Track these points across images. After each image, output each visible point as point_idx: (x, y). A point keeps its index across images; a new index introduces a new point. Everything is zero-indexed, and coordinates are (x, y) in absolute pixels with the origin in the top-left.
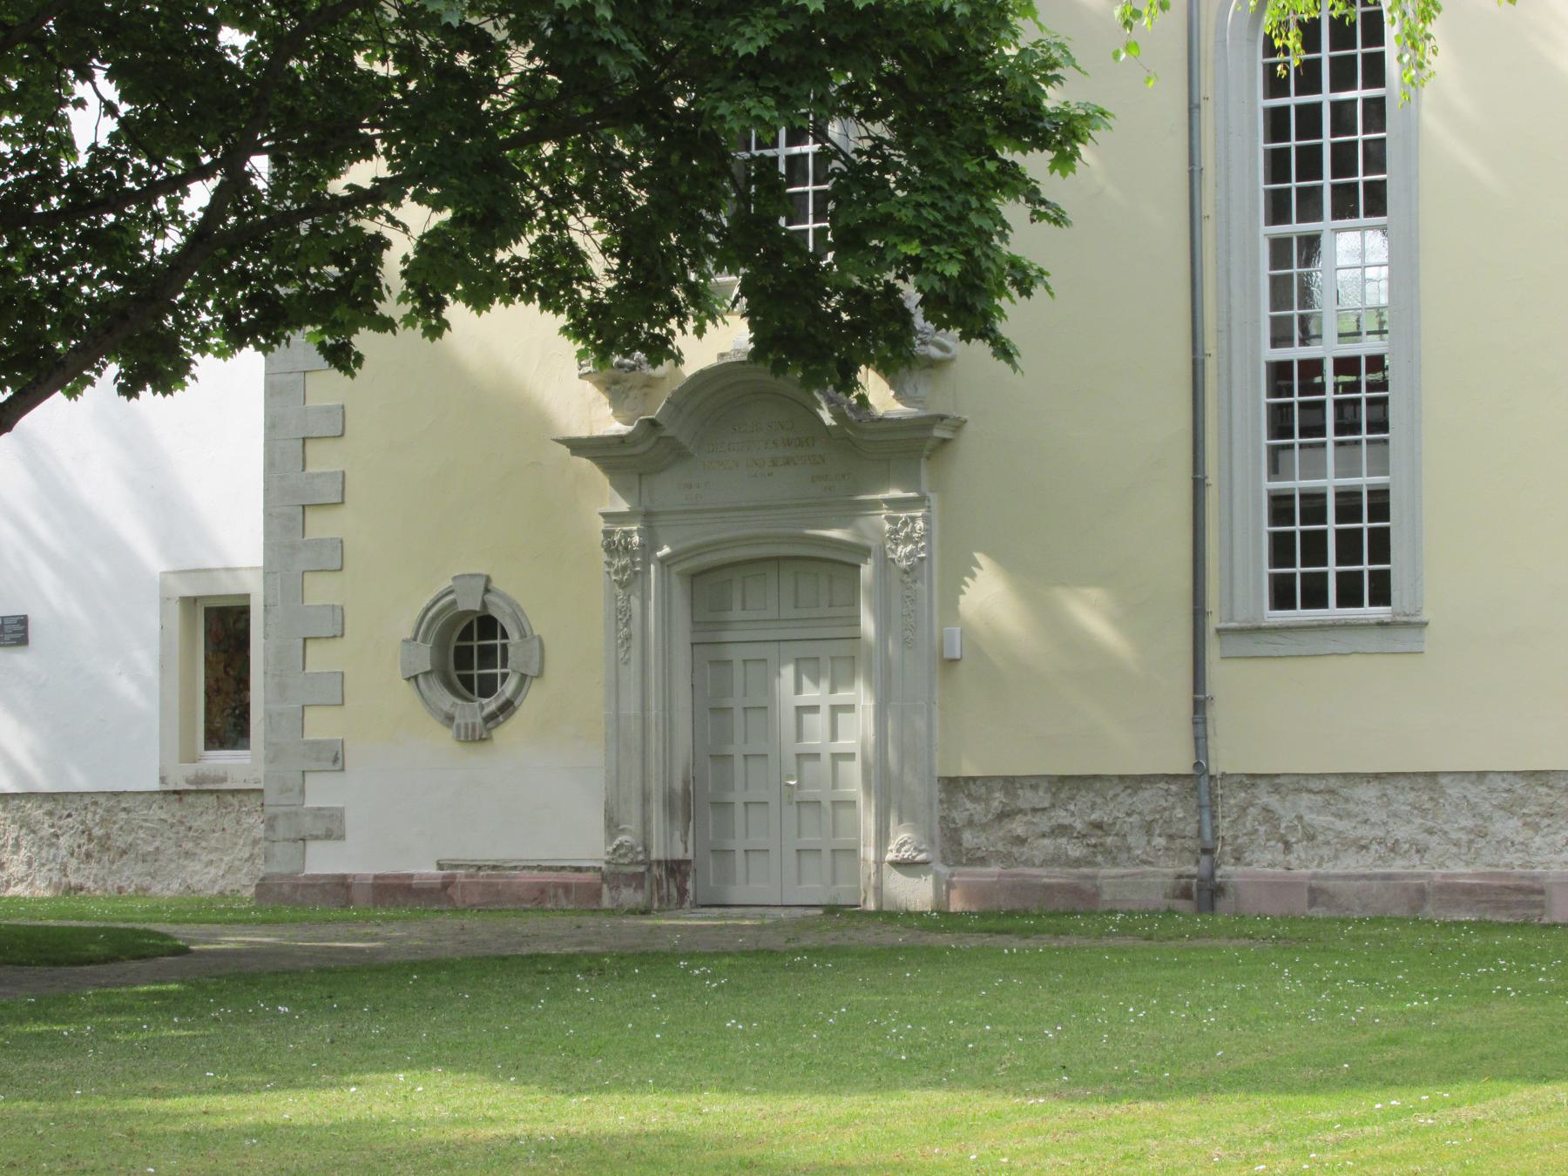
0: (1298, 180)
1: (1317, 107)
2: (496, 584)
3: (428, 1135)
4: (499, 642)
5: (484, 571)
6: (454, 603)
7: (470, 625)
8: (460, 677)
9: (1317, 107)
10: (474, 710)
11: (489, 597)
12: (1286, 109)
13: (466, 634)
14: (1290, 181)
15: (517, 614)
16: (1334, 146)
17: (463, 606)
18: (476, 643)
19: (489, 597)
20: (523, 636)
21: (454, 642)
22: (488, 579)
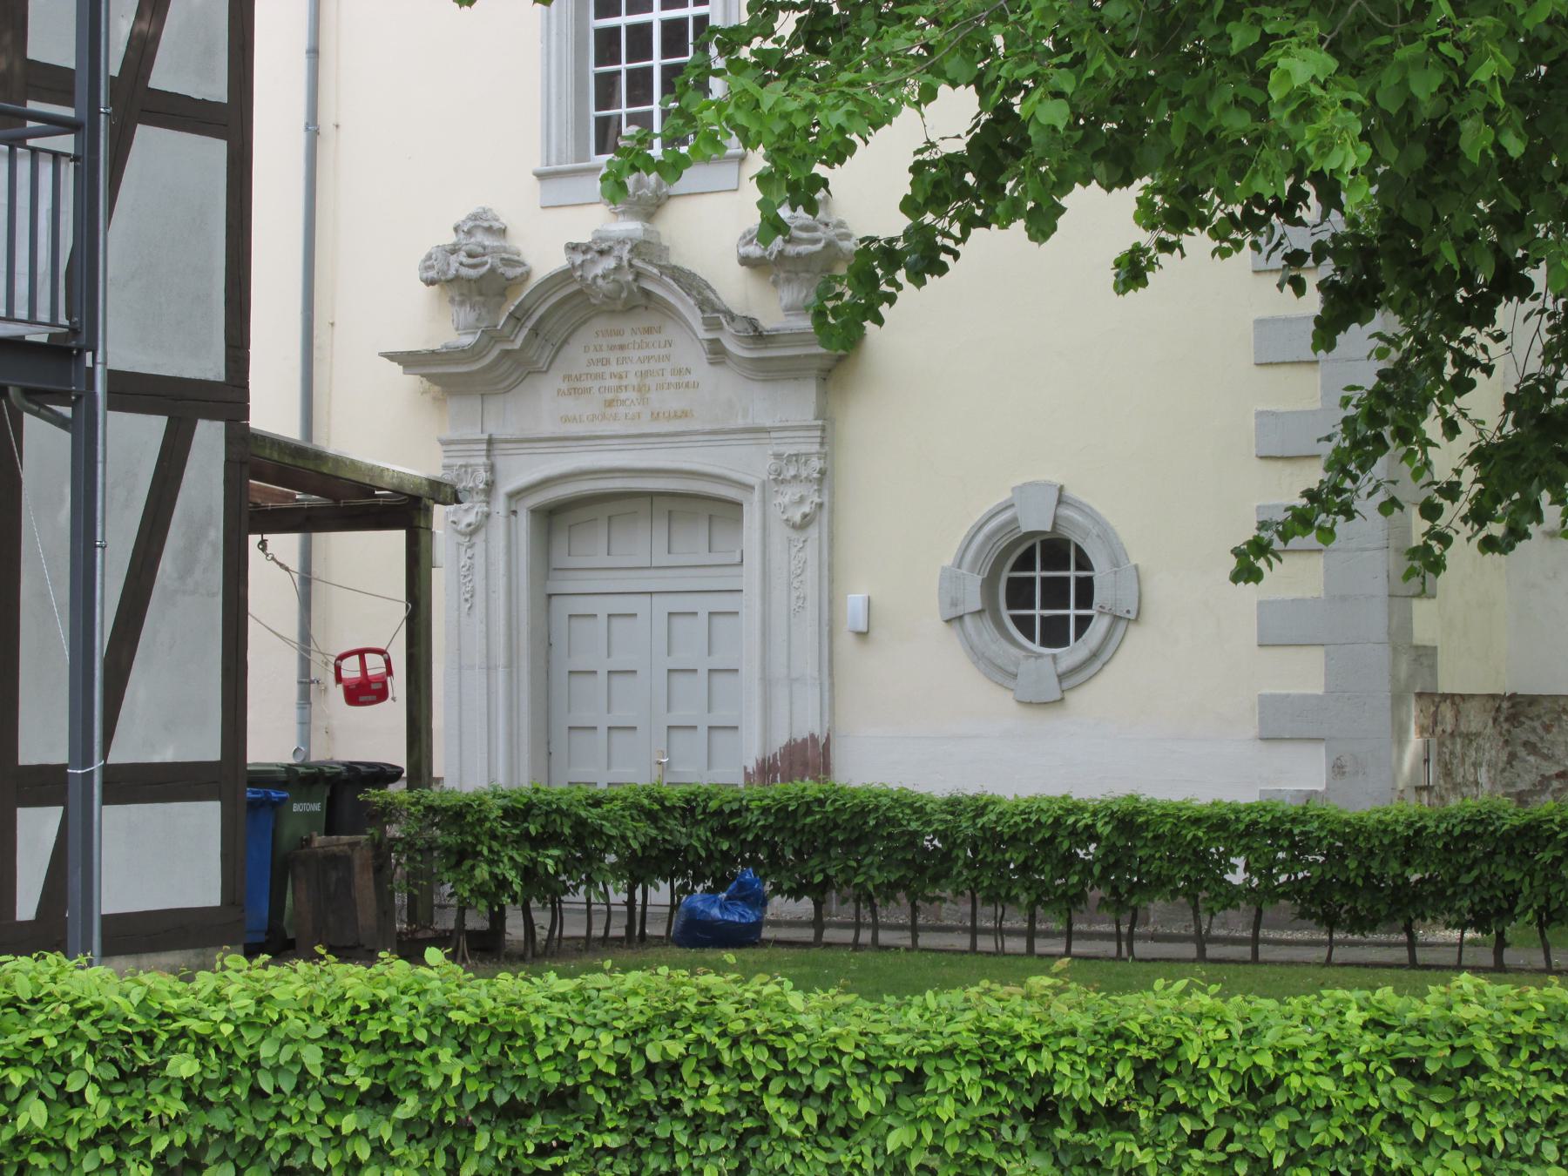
0: (628, 61)
1: (648, 27)
2: (1071, 492)
3: (1206, 811)
4: (1072, 574)
5: (1057, 480)
6: (1014, 520)
7: (1032, 549)
8: (1015, 619)
9: (648, 27)
10: (1041, 662)
11: (1065, 512)
12: (617, 29)
13: (1026, 562)
14: (620, 63)
15: (1107, 535)
16: (649, 57)
17: (1028, 525)
18: (1038, 574)
19: (1065, 512)
20: (1116, 564)
21: (1006, 574)
22: (1061, 489)
